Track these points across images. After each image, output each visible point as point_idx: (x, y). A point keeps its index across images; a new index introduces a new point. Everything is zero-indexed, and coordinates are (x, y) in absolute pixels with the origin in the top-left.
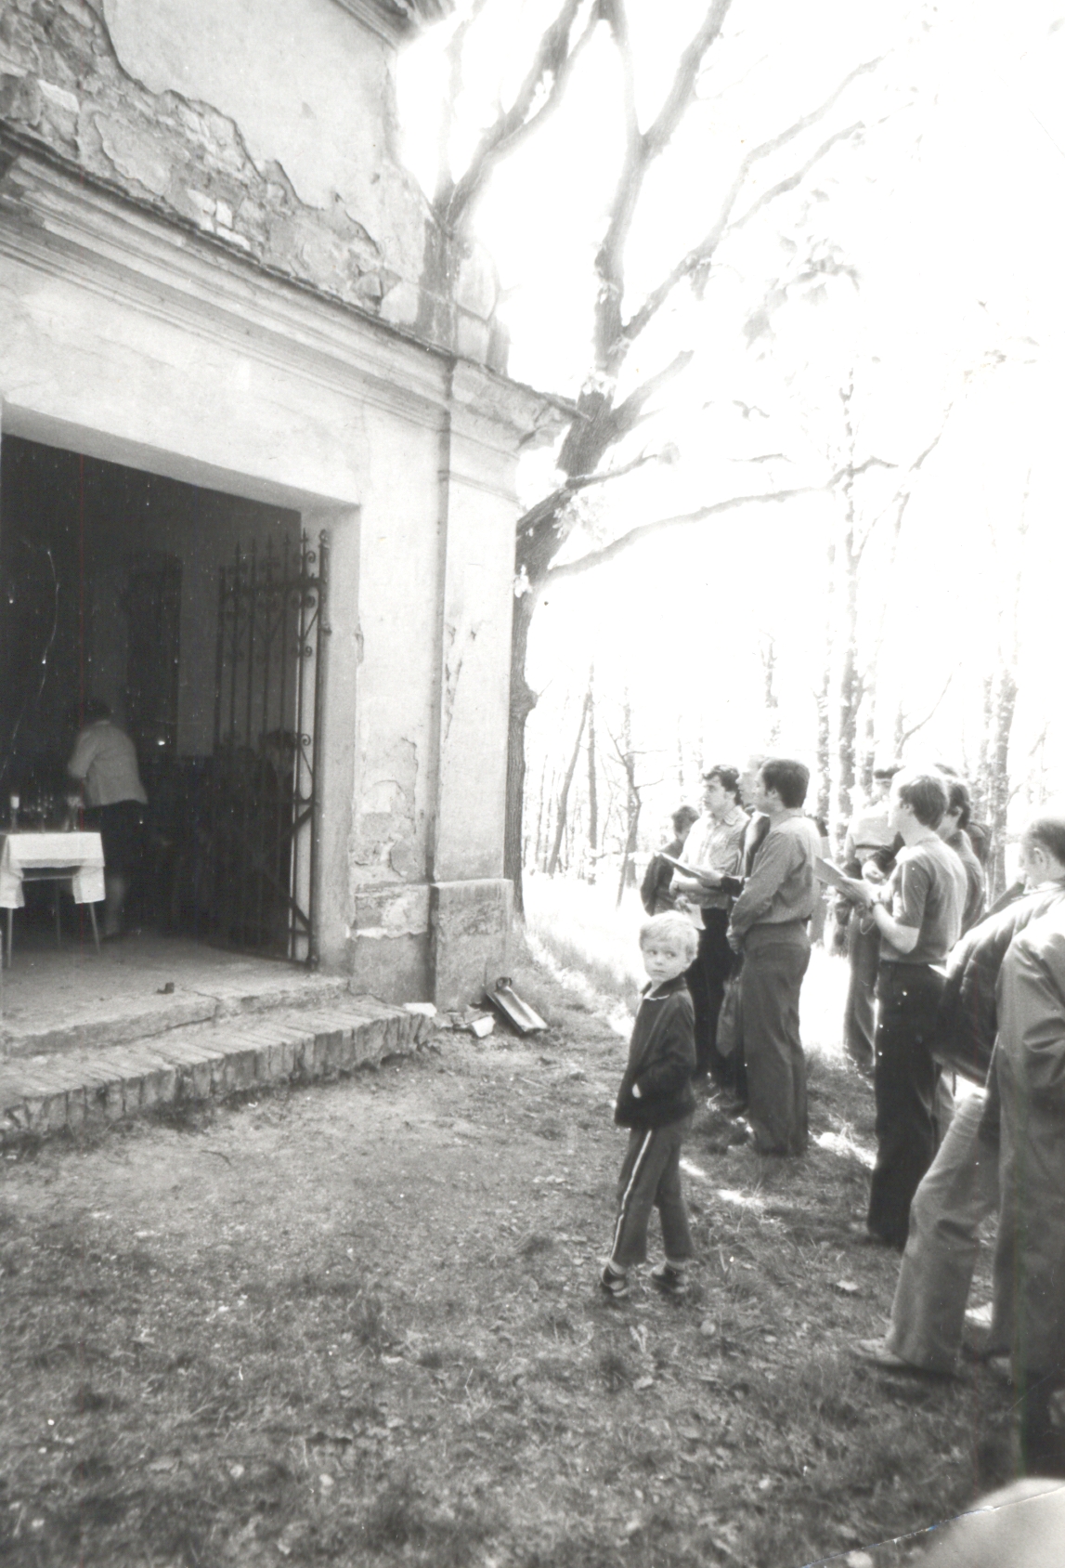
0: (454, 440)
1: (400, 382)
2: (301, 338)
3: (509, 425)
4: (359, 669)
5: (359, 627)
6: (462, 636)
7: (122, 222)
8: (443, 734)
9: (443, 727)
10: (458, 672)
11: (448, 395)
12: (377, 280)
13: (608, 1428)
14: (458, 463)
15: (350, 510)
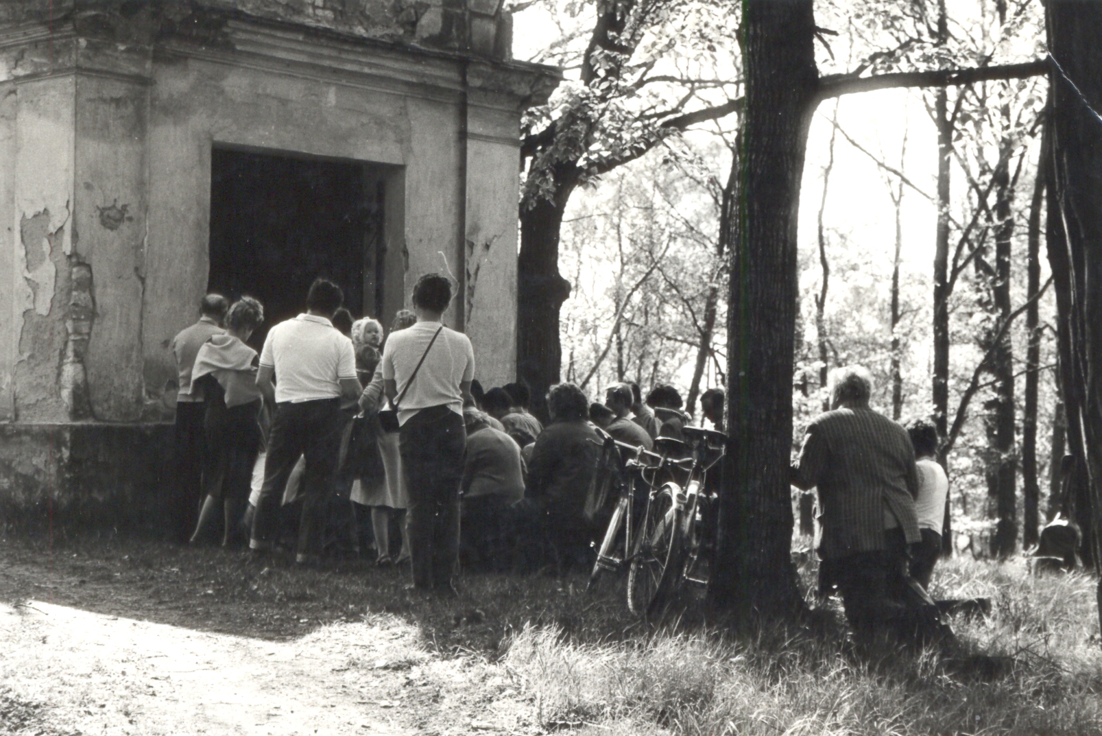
0: (470, 111)
1: (429, 82)
2: (367, 70)
3: (511, 94)
4: (405, 276)
5: (405, 246)
6: (478, 249)
7: (274, 37)
8: (466, 318)
9: (466, 314)
10: (476, 273)
11: (464, 83)
12: (412, 11)
13: (860, 350)
14: (473, 126)
15: (397, 170)
